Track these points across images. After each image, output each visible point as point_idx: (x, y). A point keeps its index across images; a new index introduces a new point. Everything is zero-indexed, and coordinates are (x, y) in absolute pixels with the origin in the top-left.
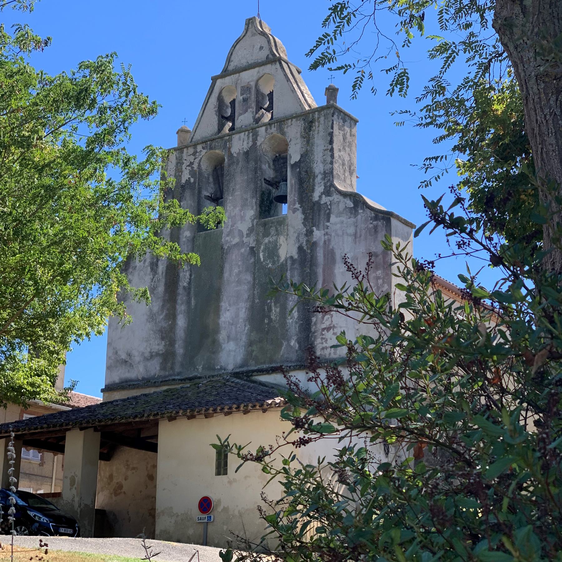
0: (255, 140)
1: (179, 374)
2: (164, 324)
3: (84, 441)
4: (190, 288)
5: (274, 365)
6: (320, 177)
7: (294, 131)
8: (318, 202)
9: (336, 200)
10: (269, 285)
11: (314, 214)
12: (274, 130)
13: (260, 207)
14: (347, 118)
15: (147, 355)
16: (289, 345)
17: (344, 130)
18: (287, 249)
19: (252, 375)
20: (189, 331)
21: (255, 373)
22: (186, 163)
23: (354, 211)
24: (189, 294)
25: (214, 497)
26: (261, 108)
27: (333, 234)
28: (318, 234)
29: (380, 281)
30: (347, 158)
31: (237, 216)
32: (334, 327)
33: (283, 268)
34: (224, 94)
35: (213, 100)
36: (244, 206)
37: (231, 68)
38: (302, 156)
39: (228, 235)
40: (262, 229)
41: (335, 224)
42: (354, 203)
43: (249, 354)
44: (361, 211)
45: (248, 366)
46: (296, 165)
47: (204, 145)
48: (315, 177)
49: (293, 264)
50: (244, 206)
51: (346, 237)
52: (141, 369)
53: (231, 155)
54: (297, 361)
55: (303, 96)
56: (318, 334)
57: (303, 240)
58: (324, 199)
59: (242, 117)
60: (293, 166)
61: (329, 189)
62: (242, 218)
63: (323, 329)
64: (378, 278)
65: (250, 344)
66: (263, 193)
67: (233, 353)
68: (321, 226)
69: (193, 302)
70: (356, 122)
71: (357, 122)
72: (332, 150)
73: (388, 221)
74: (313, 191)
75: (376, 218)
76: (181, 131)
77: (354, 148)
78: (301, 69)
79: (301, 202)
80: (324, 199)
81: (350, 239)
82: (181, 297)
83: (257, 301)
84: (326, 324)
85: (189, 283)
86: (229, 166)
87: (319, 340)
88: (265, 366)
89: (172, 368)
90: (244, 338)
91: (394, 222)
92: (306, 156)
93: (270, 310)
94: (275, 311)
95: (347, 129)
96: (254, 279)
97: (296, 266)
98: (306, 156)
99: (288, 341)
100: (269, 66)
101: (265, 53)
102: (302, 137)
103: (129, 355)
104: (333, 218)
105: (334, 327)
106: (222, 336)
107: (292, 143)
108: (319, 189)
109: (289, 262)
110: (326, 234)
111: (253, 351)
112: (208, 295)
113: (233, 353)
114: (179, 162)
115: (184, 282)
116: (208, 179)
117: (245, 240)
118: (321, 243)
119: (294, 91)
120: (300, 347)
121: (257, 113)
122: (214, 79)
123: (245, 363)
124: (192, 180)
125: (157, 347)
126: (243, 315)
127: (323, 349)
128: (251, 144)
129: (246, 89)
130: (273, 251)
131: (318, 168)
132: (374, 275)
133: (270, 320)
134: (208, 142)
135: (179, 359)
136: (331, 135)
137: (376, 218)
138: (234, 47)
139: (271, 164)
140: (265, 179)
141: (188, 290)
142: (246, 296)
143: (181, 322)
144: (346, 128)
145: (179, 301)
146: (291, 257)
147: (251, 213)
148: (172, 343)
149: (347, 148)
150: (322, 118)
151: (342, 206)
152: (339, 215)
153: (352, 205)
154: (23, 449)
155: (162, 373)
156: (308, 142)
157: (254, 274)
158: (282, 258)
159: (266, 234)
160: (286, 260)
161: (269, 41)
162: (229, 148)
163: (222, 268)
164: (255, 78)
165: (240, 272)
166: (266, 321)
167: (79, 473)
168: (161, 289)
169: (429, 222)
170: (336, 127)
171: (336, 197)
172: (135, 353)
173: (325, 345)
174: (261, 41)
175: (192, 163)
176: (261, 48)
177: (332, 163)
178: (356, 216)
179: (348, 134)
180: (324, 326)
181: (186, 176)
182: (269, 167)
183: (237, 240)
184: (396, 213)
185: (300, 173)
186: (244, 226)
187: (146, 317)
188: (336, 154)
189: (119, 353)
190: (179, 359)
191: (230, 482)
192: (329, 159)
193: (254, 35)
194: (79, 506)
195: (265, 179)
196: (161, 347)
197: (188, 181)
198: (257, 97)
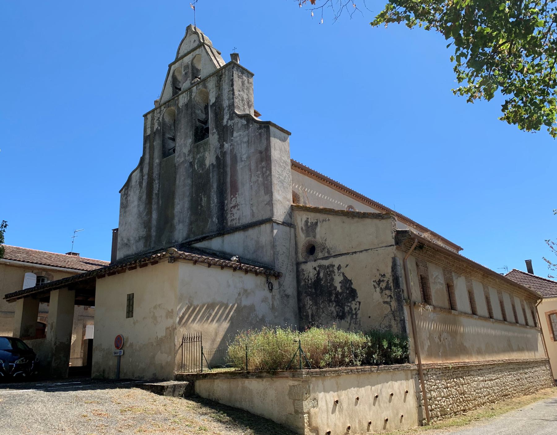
0: (191, 95)
1: (153, 248)
2: (145, 218)
3: (59, 296)
4: (158, 194)
5: (204, 235)
6: (227, 109)
7: (211, 84)
8: (226, 125)
9: (236, 121)
10: (200, 185)
11: (225, 133)
12: (200, 86)
13: (195, 136)
14: (245, 72)
15: (137, 238)
16: (212, 221)
17: (242, 79)
18: (210, 159)
19: (191, 244)
20: (159, 220)
21: (193, 242)
22: (156, 118)
23: (247, 126)
24: (158, 197)
25: (125, 335)
26: (196, 77)
27: (235, 144)
28: (226, 146)
29: (264, 169)
30: (245, 97)
31: (184, 143)
32: (238, 205)
33: (208, 172)
34: (176, 74)
35: (170, 78)
36: (186, 137)
37: (180, 55)
38: (216, 98)
39: (178, 157)
40: (196, 150)
41: (237, 137)
42: (247, 121)
43: (190, 231)
44: (251, 125)
45: (190, 238)
46: (214, 104)
47: (165, 106)
48: (224, 109)
49: (213, 168)
50: (186, 137)
51: (243, 144)
52: (134, 248)
53: (178, 108)
54: (217, 231)
55: (218, 63)
56: (228, 211)
57: (219, 151)
58: (230, 123)
59: (184, 84)
60: (211, 106)
61: (233, 115)
62: (185, 145)
63: (231, 208)
64: (263, 167)
65: (191, 223)
66: (197, 128)
67: (181, 231)
68: (228, 141)
69: (160, 202)
70: (252, 75)
71: (252, 75)
72: (233, 90)
73: (268, 128)
74: (223, 119)
75: (260, 128)
76: (156, 102)
77: (251, 92)
78: (220, 51)
79: (217, 127)
80: (230, 123)
81: (245, 145)
82: (154, 201)
83: (194, 195)
84: (233, 204)
85: (158, 191)
86: (178, 115)
87: (229, 215)
88: (199, 237)
89: (150, 245)
90: (187, 220)
91: (272, 129)
92: (219, 98)
93: (201, 200)
94: (204, 199)
95: (245, 78)
96: (192, 182)
97: (215, 169)
98: (219, 98)
99: (212, 218)
100: (198, 50)
101: (197, 43)
102: (216, 86)
103: (128, 240)
104: (235, 134)
105: (238, 205)
106: (176, 220)
107: (211, 92)
108: (226, 117)
109: (211, 167)
110: (231, 145)
111: (192, 228)
112: (168, 197)
113: (181, 231)
114: (153, 119)
115: (155, 191)
116: (171, 127)
117: (187, 158)
118: (229, 152)
119: (211, 60)
120: (218, 221)
121: (192, 80)
122: (170, 66)
123: (188, 237)
124: (159, 128)
125: (142, 233)
126: (187, 205)
127: (232, 220)
128: (189, 98)
129: (187, 67)
130: (202, 163)
131: (226, 103)
132: (260, 166)
133: (202, 206)
134: (167, 104)
135: (153, 239)
136: (232, 80)
137: (260, 128)
138: (181, 45)
139: (204, 110)
140: (198, 120)
141: (157, 195)
142: (188, 194)
143: (154, 216)
144: (244, 77)
145: (153, 203)
146: (212, 164)
147: (190, 141)
148: (149, 229)
149: (245, 91)
150: (227, 72)
151: (240, 125)
152: (239, 130)
153: (246, 123)
154: (40, 304)
155: (145, 249)
156: (219, 89)
157: (192, 179)
158: (207, 166)
159: (198, 153)
160: (209, 166)
161: (198, 36)
162: (178, 104)
163: (175, 178)
164: (191, 59)
165: (185, 179)
166: (199, 208)
167: (55, 321)
168: (144, 197)
169: (393, 245)
170: (235, 76)
171: (236, 120)
172: (132, 239)
173: (233, 218)
174: (194, 37)
175: (159, 118)
176: (195, 41)
177: (233, 98)
178: (248, 129)
179: (246, 82)
180: (232, 205)
181: (156, 126)
182: (202, 112)
183: (183, 159)
184: (273, 121)
185: (215, 109)
186: (186, 150)
187: (137, 215)
188: (236, 93)
189: (124, 239)
190: (153, 239)
191: (134, 323)
192: (231, 96)
193: (190, 35)
194: (55, 344)
195: (198, 120)
196: (144, 233)
197: (157, 129)
198: (192, 70)
